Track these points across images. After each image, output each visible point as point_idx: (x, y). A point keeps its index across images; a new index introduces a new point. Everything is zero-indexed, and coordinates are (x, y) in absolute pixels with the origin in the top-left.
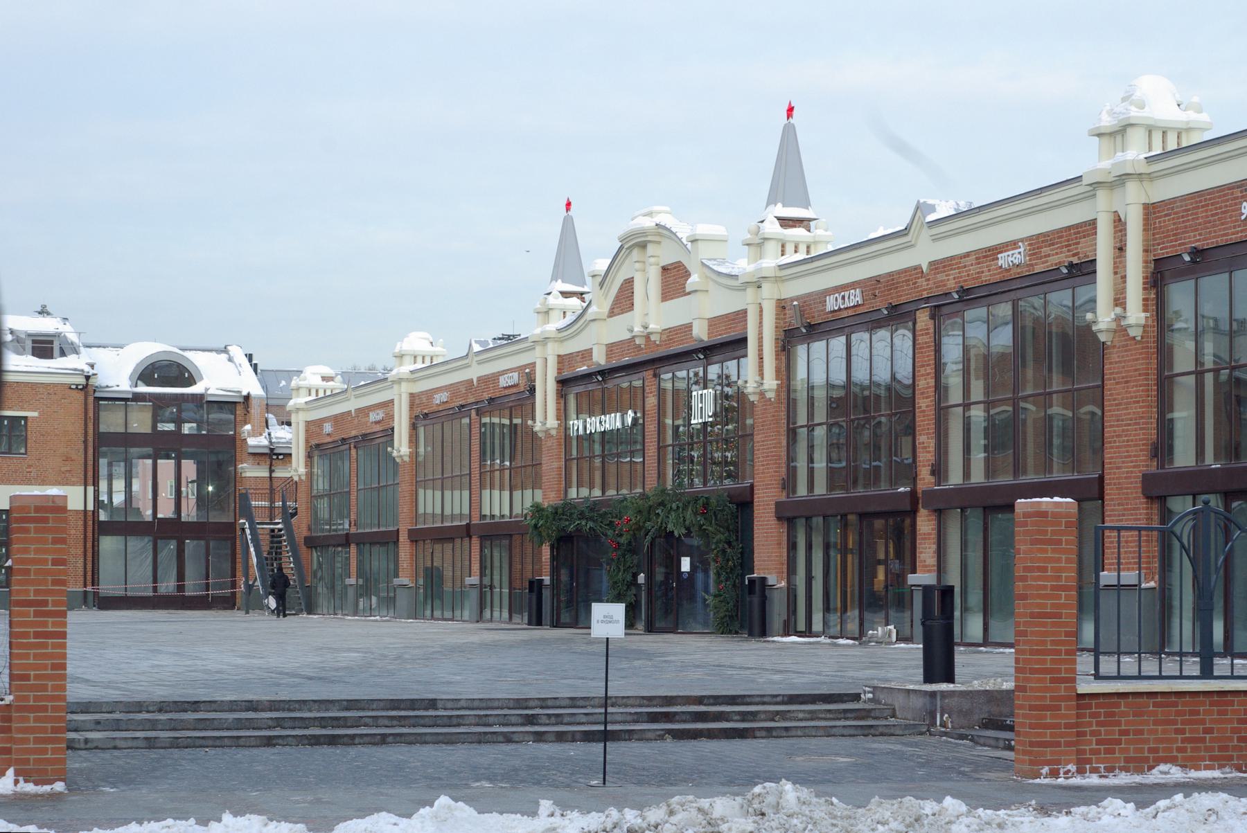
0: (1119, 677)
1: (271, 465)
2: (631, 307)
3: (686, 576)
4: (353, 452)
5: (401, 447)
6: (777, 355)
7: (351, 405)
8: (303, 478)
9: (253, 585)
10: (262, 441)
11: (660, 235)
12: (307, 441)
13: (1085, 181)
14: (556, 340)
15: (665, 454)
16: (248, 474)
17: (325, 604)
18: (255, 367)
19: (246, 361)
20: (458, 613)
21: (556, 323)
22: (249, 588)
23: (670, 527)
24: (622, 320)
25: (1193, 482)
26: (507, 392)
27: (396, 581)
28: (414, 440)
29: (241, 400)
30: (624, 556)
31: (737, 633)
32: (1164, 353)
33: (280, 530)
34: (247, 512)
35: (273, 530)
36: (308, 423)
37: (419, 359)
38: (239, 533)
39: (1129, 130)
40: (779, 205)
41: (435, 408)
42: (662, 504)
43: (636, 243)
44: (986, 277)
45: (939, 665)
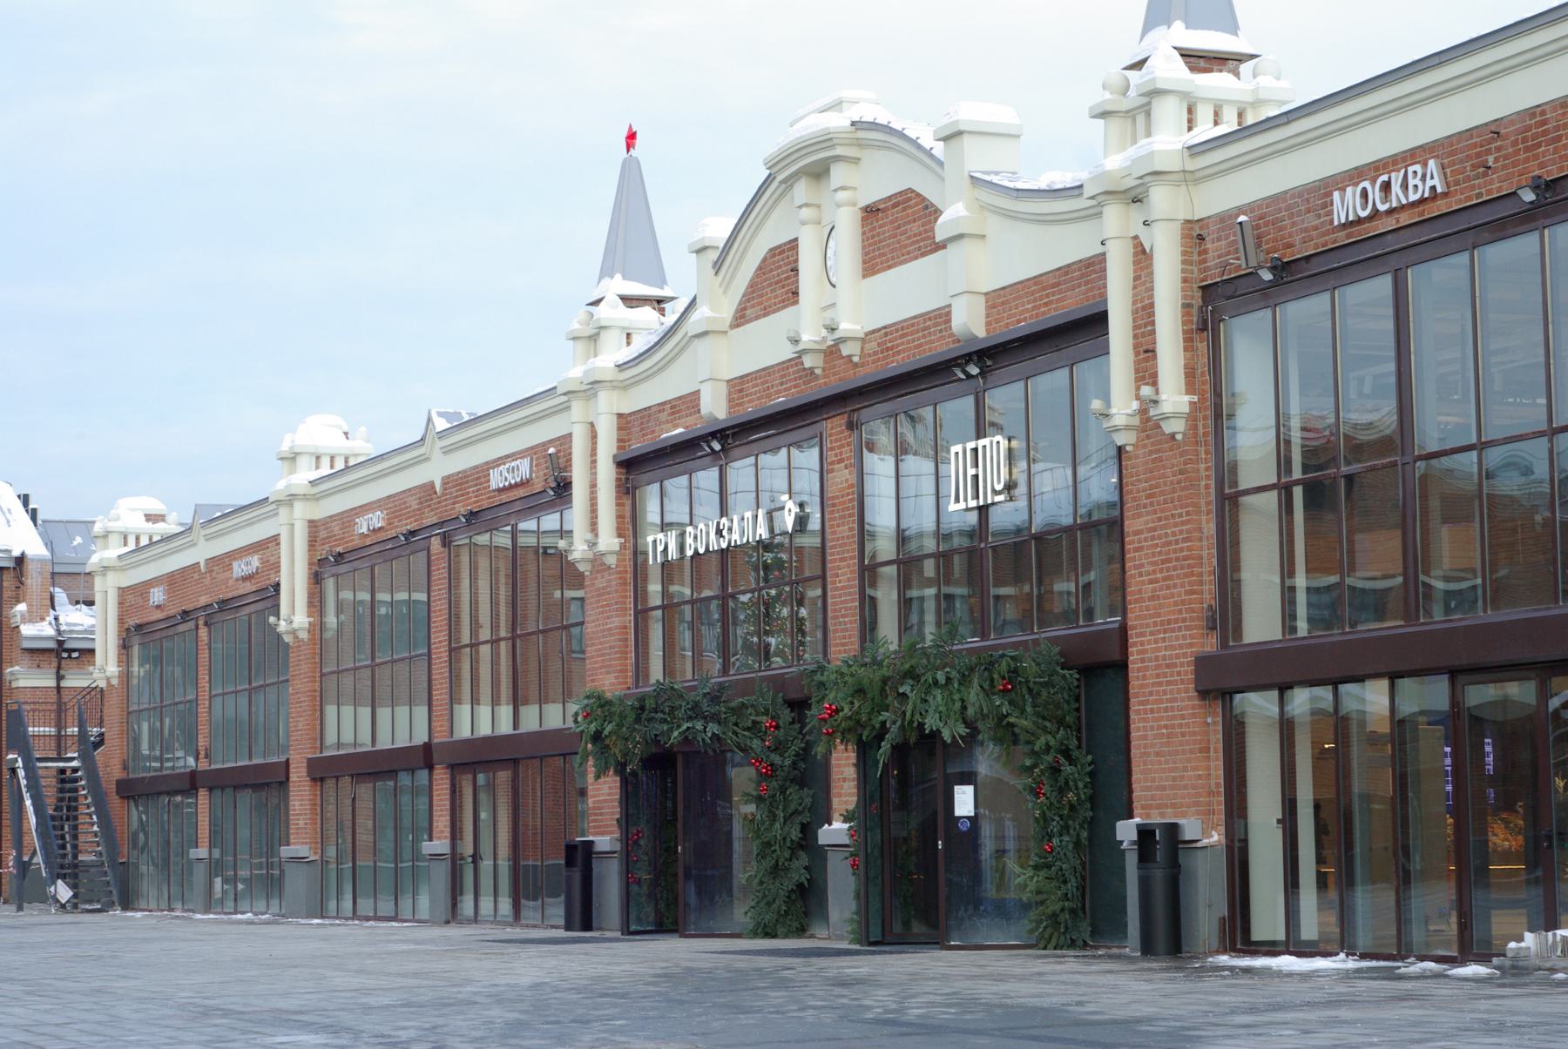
1: (59, 668)
2: (793, 296)
3: (965, 826)
4: (203, 632)
5: (294, 616)
6: (618, 498)
7: (199, 553)
8: (115, 682)
9: (29, 863)
10: (45, 629)
11: (860, 144)
12: (121, 621)
13: (1088, 192)
14: (615, 386)
15: (458, 661)
16: (22, 683)
17: (153, 892)
18: (33, 515)
19: (19, 504)
20: (405, 903)
21: (613, 353)
22: (24, 867)
23: (931, 722)
24: (780, 322)
25: (1280, 669)
26: (505, 498)
27: (285, 852)
28: (316, 602)
29: (11, 564)
30: (783, 790)
31: (1085, 945)
33: (75, 770)
34: (22, 744)
35: (62, 771)
36: (123, 591)
37: (325, 461)
38: (6, 776)
39: (603, 334)
40: (618, 276)
41: (357, 543)
42: (912, 675)
43: (808, 166)
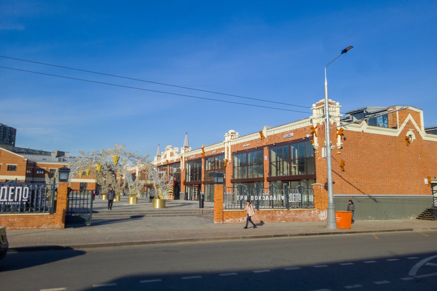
0: (232, 209)
28: (139, 174)
32: (234, 165)
44: (211, 154)
45: (202, 206)
